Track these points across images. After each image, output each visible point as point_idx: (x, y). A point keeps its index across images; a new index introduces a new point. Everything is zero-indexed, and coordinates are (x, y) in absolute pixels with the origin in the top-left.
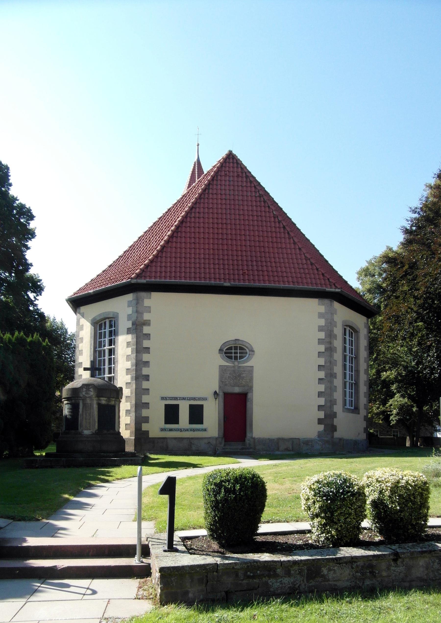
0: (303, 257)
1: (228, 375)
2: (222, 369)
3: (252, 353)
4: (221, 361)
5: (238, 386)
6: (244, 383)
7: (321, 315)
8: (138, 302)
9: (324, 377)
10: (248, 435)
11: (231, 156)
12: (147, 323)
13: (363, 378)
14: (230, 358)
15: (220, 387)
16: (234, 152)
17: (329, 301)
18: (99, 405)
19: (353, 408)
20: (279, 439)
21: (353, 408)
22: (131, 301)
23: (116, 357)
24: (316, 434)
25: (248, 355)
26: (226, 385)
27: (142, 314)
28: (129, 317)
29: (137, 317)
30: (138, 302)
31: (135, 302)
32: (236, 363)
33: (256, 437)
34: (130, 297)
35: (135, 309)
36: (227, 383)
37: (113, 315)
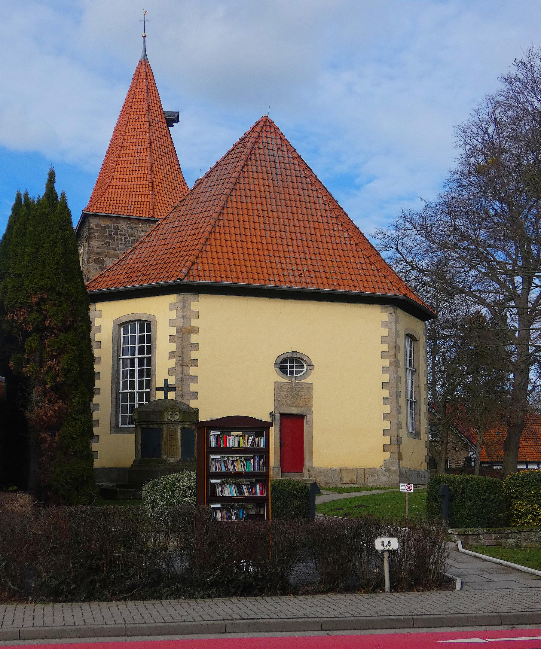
0: (361, 255)
1: (285, 393)
2: (278, 386)
3: (311, 368)
4: (277, 377)
5: (296, 406)
6: (302, 403)
7: (384, 325)
8: (185, 306)
9: (389, 397)
10: (307, 464)
11: (268, 124)
12: (195, 330)
13: (425, 396)
14: (285, 372)
15: (276, 407)
16: (271, 118)
17: (392, 308)
18: (182, 429)
19: (414, 432)
20: (342, 470)
21: (414, 432)
22: (175, 303)
23: (153, 369)
24: (382, 463)
25: (305, 370)
26: (282, 405)
27: (190, 319)
28: (172, 322)
29: (183, 324)
30: (185, 306)
31: (179, 305)
32: (294, 380)
33: (317, 467)
34: (173, 298)
35: (180, 314)
36: (284, 402)
37: (148, 317)
